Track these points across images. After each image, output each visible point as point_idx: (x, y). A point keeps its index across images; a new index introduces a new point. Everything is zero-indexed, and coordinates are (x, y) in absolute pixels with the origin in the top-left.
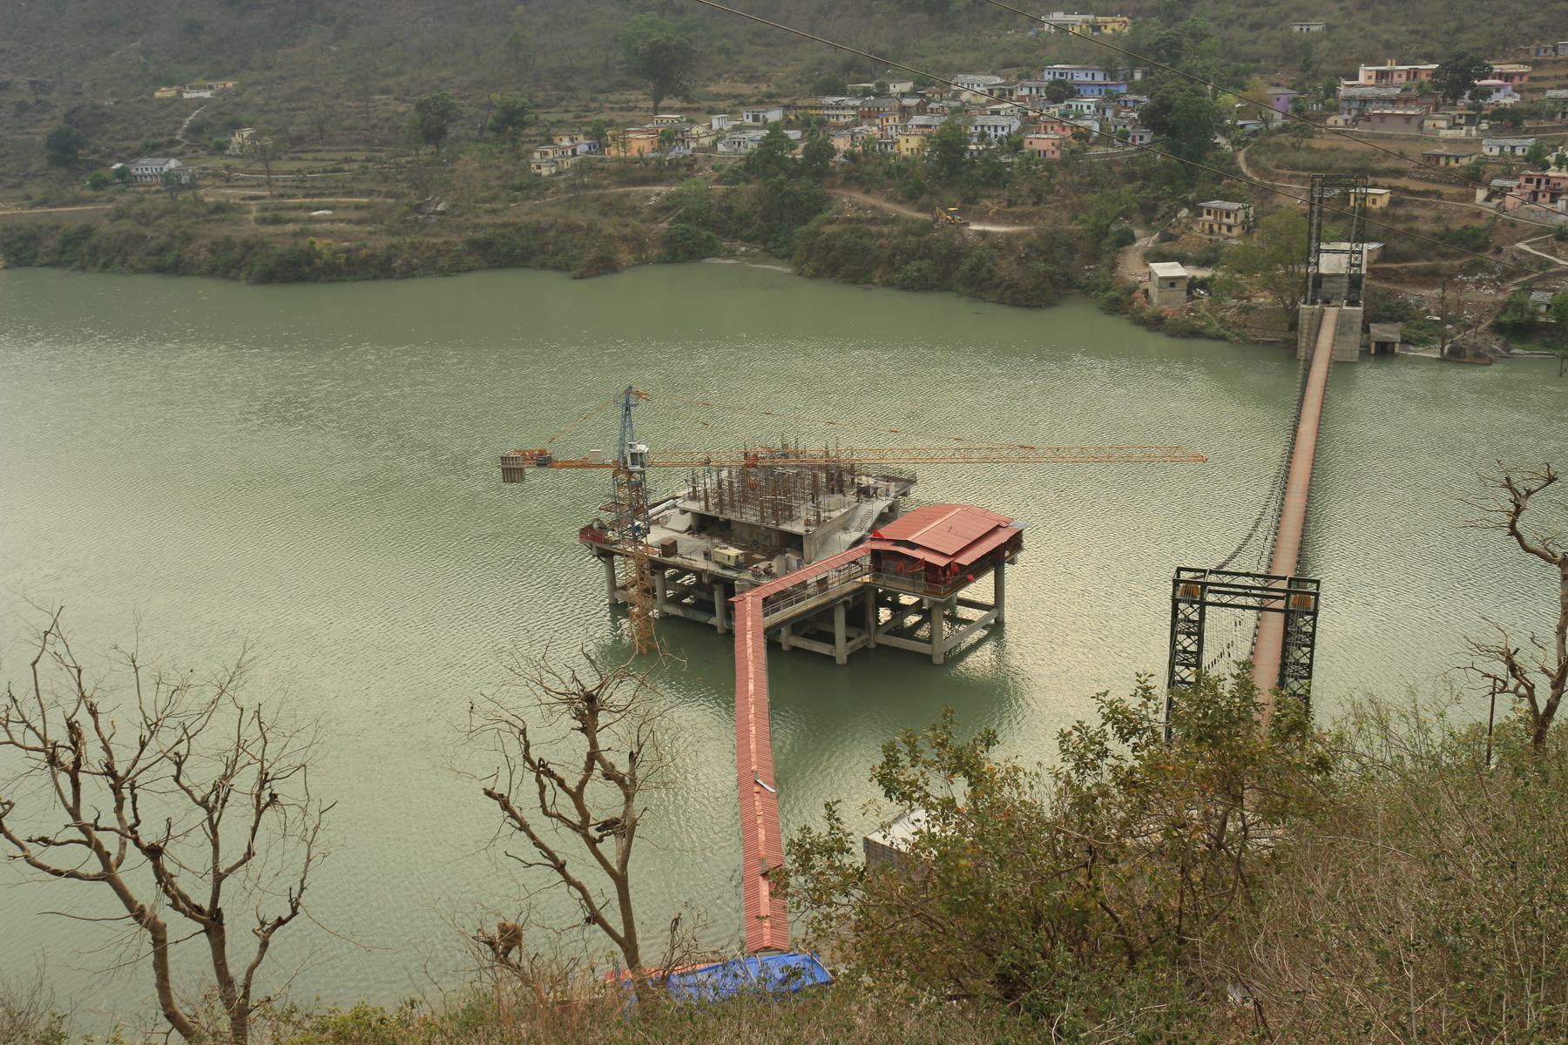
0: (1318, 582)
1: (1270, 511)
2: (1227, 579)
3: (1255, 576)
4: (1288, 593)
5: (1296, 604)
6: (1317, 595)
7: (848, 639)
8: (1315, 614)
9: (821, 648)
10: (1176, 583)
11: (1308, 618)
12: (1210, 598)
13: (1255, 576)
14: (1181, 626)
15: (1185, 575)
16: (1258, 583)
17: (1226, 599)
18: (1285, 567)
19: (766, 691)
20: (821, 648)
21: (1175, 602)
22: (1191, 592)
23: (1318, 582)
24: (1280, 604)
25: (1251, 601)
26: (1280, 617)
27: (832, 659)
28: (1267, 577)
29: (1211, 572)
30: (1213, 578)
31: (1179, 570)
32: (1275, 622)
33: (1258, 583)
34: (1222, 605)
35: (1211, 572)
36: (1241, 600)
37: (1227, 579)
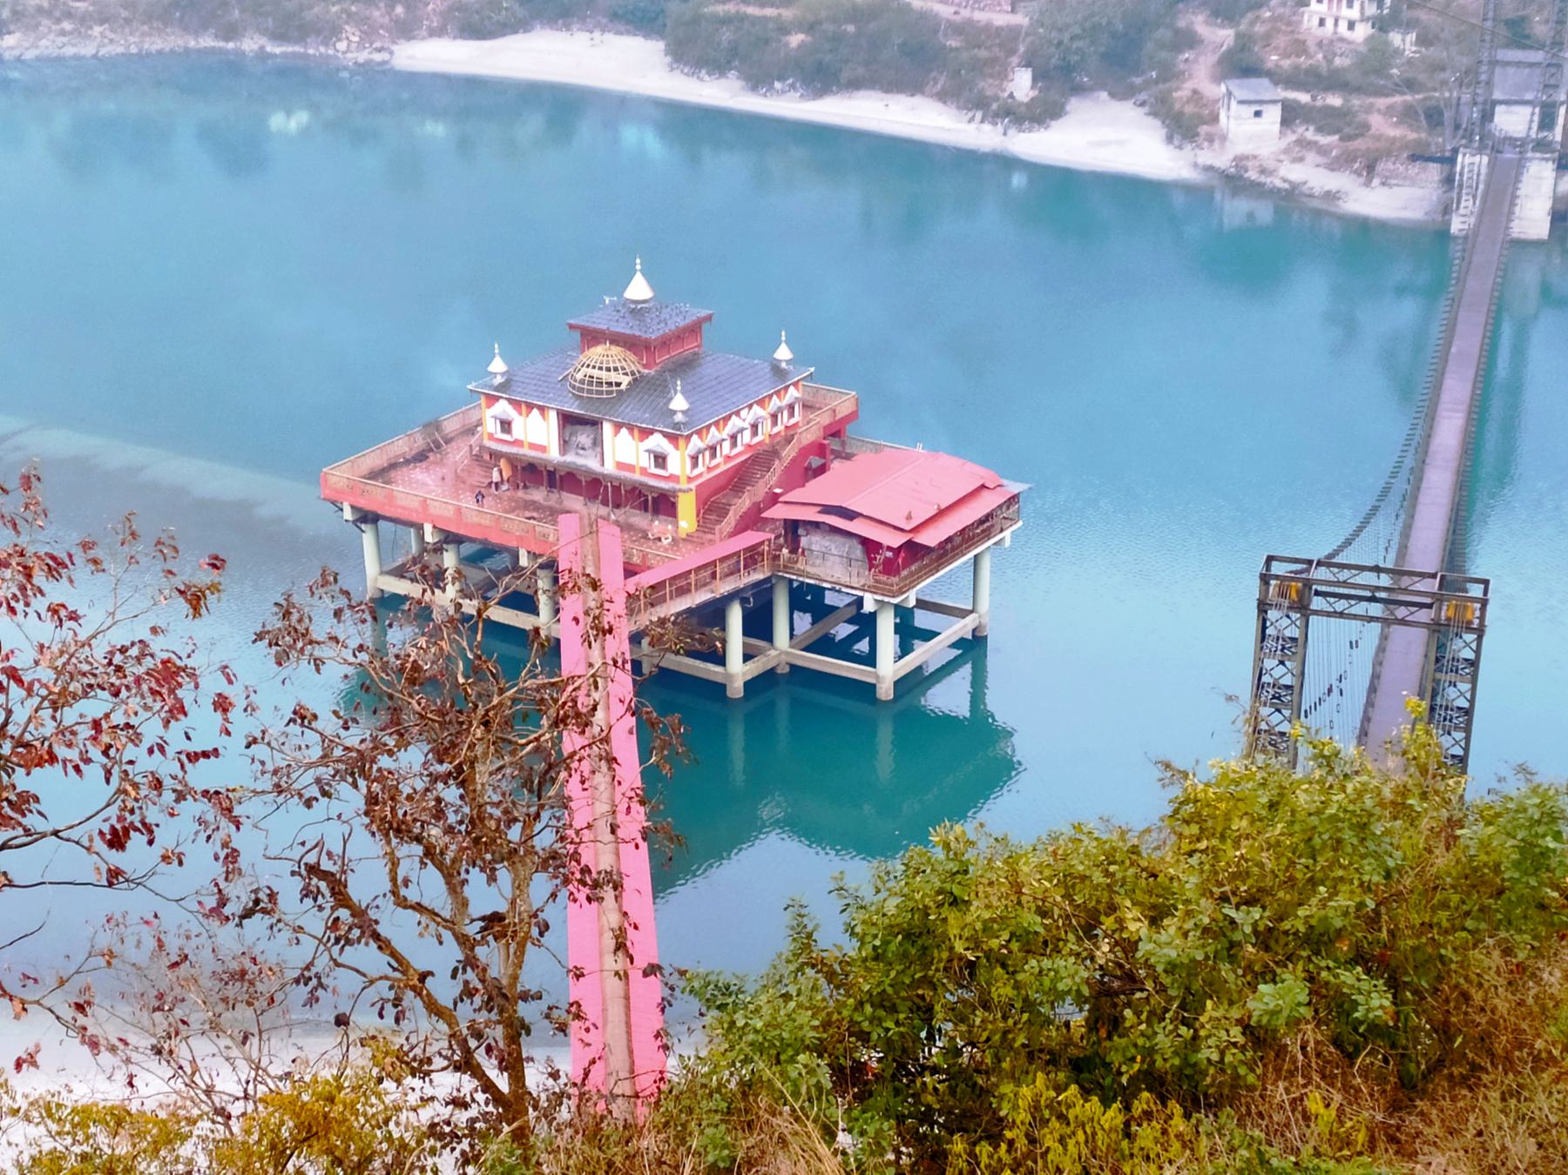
0: (1486, 582)
1: (1404, 473)
2: (1344, 575)
3: (1377, 569)
4: (1438, 599)
5: (1446, 614)
6: (1484, 603)
7: (747, 657)
8: (1480, 632)
9: (710, 670)
10: (1265, 579)
11: (1470, 637)
12: (1317, 603)
13: (1377, 569)
14: (1269, 643)
15: (1278, 568)
16: (1385, 580)
17: (1341, 605)
18: (1426, 553)
19: (1479, 506)
20: (710, 670)
21: (1263, 607)
22: (1291, 593)
23: (1486, 582)
24: (1424, 616)
25: (1376, 609)
26: (1420, 635)
27: (717, 690)
28: (1396, 573)
29: (1319, 563)
30: (1321, 573)
31: (1270, 559)
32: (1411, 644)
33: (1385, 580)
34: (1341, 615)
35: (1319, 563)
36: (1360, 608)
37: (1344, 575)
